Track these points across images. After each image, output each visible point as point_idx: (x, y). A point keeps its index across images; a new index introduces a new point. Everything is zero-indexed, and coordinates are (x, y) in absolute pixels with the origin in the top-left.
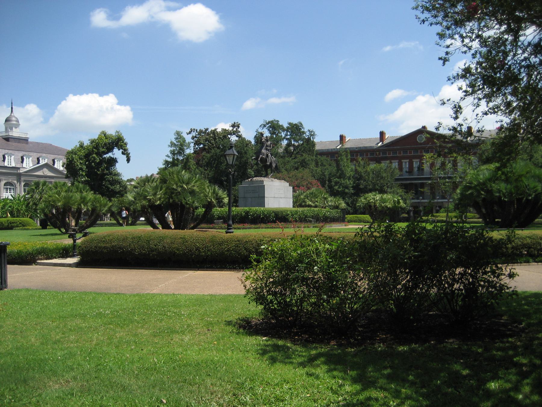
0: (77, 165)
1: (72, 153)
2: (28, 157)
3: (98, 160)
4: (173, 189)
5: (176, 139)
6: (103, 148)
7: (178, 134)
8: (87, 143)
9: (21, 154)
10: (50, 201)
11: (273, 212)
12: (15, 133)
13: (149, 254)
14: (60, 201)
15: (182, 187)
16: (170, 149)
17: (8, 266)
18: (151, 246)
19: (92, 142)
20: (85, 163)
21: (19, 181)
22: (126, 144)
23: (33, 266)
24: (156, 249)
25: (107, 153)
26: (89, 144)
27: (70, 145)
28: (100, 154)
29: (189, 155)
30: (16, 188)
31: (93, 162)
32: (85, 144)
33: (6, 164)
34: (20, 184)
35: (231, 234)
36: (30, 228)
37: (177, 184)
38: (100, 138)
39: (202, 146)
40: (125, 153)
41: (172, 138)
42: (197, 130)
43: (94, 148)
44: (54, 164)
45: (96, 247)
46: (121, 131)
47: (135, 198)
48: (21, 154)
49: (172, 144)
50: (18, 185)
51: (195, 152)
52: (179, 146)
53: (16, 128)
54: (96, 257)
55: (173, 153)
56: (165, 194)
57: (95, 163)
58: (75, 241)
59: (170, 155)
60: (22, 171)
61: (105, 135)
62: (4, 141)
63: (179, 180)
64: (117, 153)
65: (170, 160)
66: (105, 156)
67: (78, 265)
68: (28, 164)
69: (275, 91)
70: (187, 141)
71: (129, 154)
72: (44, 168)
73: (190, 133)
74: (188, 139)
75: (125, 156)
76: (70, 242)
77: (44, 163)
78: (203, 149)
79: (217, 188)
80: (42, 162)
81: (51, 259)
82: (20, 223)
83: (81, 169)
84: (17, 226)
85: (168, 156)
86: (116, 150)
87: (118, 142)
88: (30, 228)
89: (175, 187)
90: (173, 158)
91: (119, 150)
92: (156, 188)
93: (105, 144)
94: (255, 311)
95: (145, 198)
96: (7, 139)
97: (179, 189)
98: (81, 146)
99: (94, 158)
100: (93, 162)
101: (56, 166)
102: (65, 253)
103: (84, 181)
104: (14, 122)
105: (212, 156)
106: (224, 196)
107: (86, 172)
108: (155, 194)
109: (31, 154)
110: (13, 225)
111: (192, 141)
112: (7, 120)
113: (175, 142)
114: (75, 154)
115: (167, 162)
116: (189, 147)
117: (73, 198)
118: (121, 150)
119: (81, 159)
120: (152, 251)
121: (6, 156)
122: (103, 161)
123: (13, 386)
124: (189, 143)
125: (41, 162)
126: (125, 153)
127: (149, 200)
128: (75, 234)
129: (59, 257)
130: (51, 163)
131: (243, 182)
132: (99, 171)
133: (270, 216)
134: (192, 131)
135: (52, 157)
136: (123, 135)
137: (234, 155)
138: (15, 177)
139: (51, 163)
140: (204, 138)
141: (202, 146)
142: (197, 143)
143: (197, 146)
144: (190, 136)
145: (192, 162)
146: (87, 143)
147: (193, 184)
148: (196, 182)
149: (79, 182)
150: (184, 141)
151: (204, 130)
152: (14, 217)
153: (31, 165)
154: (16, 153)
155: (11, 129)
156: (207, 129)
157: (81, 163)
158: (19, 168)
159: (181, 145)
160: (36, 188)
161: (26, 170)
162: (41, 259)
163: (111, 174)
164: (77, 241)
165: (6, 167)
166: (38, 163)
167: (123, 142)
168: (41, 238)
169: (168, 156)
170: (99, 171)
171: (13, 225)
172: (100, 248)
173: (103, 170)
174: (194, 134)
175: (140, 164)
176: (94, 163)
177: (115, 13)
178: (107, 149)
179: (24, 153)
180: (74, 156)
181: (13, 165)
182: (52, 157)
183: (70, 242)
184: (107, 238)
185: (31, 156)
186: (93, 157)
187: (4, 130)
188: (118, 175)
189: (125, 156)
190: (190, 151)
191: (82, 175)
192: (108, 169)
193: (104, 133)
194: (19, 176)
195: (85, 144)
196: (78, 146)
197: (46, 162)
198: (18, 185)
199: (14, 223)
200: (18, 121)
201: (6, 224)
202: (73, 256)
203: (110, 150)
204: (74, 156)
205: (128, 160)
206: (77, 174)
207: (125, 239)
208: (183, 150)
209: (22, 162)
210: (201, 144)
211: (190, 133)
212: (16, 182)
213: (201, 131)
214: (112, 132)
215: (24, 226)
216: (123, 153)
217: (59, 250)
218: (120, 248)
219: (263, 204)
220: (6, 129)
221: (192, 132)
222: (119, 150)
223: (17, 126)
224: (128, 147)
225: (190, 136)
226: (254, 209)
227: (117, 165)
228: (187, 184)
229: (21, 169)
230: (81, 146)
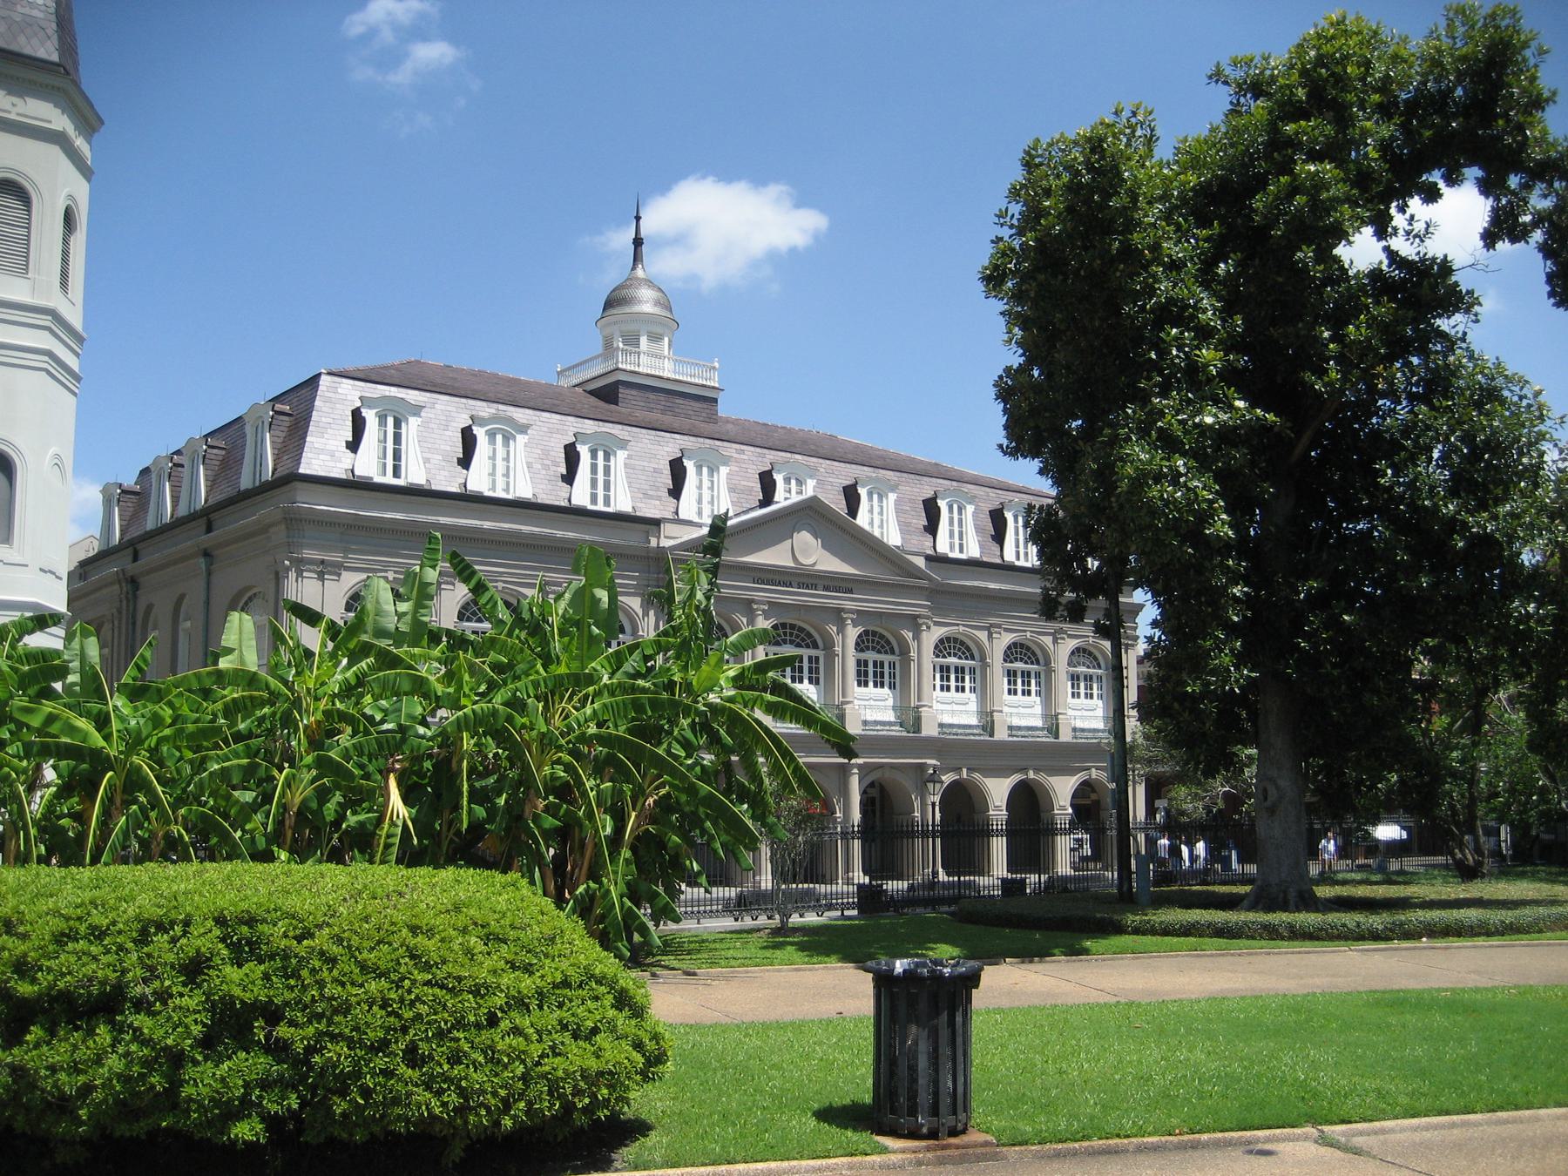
20: (1209, 264)
33: (580, 495)
36: (1438, 1020)
44: (853, 510)
48: (670, 446)
60: (671, 537)
62: (593, 400)
69: (246, 1130)
72: (796, 528)
77: (795, 498)
80: (785, 497)
101: (862, 520)
103: (1224, 436)
109: (730, 449)
125: (780, 495)
136: (1525, 24)
149: (1169, 444)
154: (644, 440)
155: (632, 340)
158: (656, 523)
166: (767, 500)
168: (676, 425)
181: (622, 502)
182: (845, 474)
185: (726, 461)
191: (1193, 370)
220: (608, 345)
229: (667, 529)
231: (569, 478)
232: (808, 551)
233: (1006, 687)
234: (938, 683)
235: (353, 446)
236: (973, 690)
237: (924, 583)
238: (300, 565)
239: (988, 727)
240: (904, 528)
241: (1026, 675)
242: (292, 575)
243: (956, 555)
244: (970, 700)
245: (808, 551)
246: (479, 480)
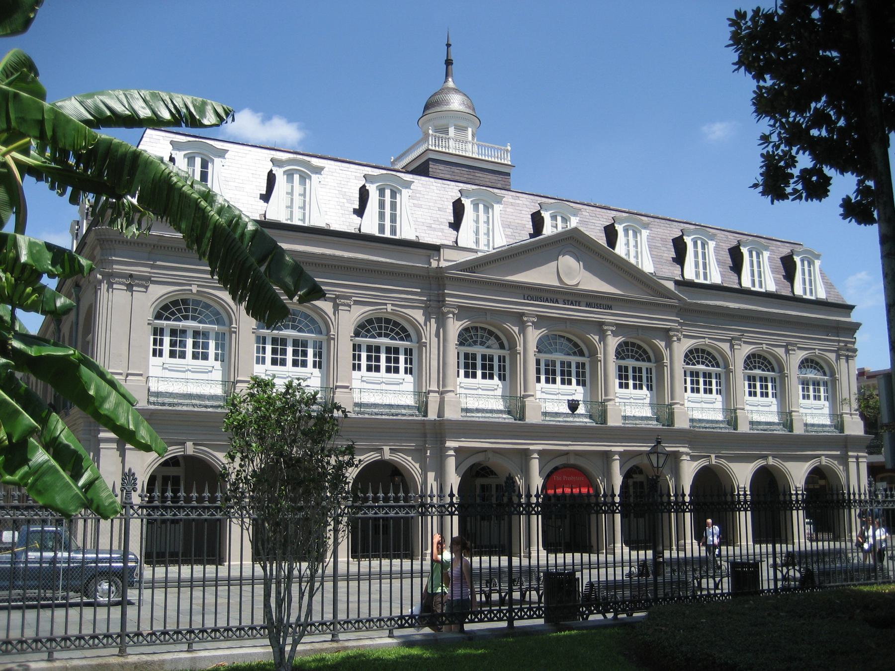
21: (436, 309)
34: (442, 323)
60: (448, 259)
138: (414, 293)
158: (436, 249)
161: (471, 256)
193: (740, 63)
212: (418, 315)
229: (446, 254)
233: (801, 393)
234: (689, 386)
236: (719, 392)
237: (674, 302)
238: (110, 277)
239: (733, 422)
241: (764, 379)
242: (104, 286)
244: (772, 403)
245: (571, 272)
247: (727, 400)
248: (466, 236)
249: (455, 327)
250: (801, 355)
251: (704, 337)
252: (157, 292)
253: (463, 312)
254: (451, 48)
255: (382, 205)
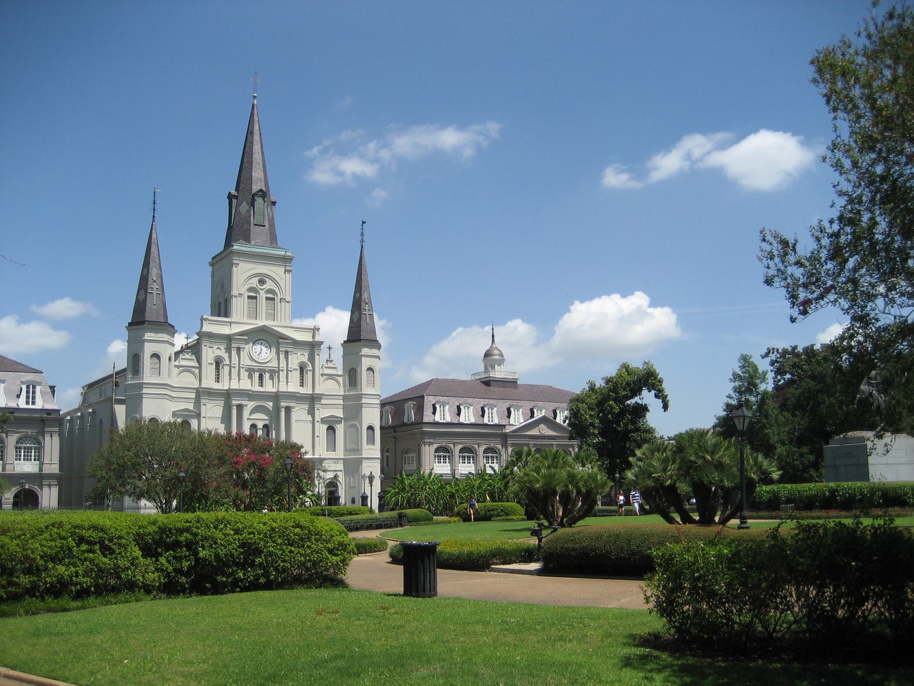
0: (586, 419)
1: (577, 400)
2: (517, 408)
3: (617, 410)
4: (691, 461)
5: (742, 367)
6: (625, 389)
7: (745, 361)
8: (599, 383)
9: (506, 404)
10: (525, 482)
11: (879, 489)
12: (499, 373)
13: (630, 558)
14: (538, 481)
15: (704, 458)
16: (733, 384)
17: (439, 571)
18: (632, 547)
19: (608, 381)
21: (505, 445)
22: (660, 381)
23: (487, 573)
24: (638, 552)
25: (632, 397)
26: (603, 385)
27: (578, 387)
28: (620, 400)
29: (765, 393)
30: (500, 455)
31: (609, 413)
32: (598, 386)
33: (486, 421)
34: (506, 449)
35: (745, 530)
36: (515, 518)
37: (696, 454)
38: (619, 376)
39: (788, 376)
40: (660, 395)
41: (736, 367)
42: (778, 350)
43: (611, 390)
44: (555, 417)
45: (561, 548)
46: (652, 362)
47: (636, 476)
48: (506, 404)
49: (736, 377)
50: (503, 451)
51: (777, 388)
52: (748, 379)
53: (499, 365)
54: (561, 563)
55: (738, 390)
56: (680, 468)
57: (613, 414)
58: (540, 541)
59: (733, 395)
60: (508, 430)
61: (627, 370)
63: (700, 447)
64: (647, 397)
65: (734, 402)
66: (629, 402)
67: (539, 573)
68: (518, 419)
70: (760, 371)
71: (666, 397)
73: (767, 355)
74: (764, 366)
75: (660, 401)
76: (534, 541)
77: (540, 416)
78: (791, 382)
79: (760, 458)
80: (538, 415)
81: (510, 563)
82: (502, 511)
83: (592, 425)
84: (498, 515)
85: (729, 397)
86: (645, 392)
87: (648, 379)
88: (515, 518)
89: (693, 458)
90: (739, 401)
91: (650, 391)
92: (665, 461)
93: (628, 384)
94: (658, 624)
95: (650, 476)
96: (487, 383)
97: (700, 462)
98: (592, 388)
99: (611, 406)
100: (609, 413)
102: (527, 555)
104: (497, 357)
105: (803, 393)
106: (772, 469)
107: (599, 429)
108: (664, 470)
110: (492, 513)
111: (772, 368)
112: (487, 355)
113: (740, 373)
114: (583, 402)
115: (729, 407)
116: (764, 378)
117: (557, 477)
118: (653, 392)
119: (590, 409)
120: (634, 554)
121: (486, 409)
122: (625, 410)
123: (392, 668)
124: (765, 373)
126: (660, 395)
127: (657, 480)
128: (540, 531)
129: (520, 562)
130: (551, 416)
131: (831, 441)
132: (620, 426)
133: (872, 495)
134: (769, 352)
135: (553, 406)
137: (744, 417)
138: (499, 440)
139: (551, 416)
140: (791, 363)
141: (788, 376)
142: (779, 372)
143: (779, 377)
144: (768, 360)
145: (771, 404)
146: (599, 383)
147: (721, 453)
148: (725, 450)
149: (589, 445)
150: (756, 369)
151: (790, 349)
152: (495, 501)
153: (522, 420)
155: (493, 368)
156: (795, 348)
157: (591, 415)
158: (504, 426)
159: (751, 377)
160: (517, 459)
161: (514, 428)
162: (497, 564)
163: (637, 430)
164: (543, 540)
165: (486, 425)
166: (532, 416)
167: (655, 378)
169: (729, 397)
170: (620, 426)
171: (492, 513)
172: (567, 549)
173: (626, 425)
174: (773, 357)
175: (687, 410)
176: (612, 414)
177: (639, 169)
178: (630, 391)
179: (511, 402)
180: (580, 405)
182: (553, 406)
183: (534, 541)
184: (576, 536)
185: (521, 407)
186: (609, 405)
187: (482, 368)
188: (650, 431)
189: (660, 401)
190: (767, 386)
192: (634, 422)
193: (626, 367)
194: (504, 438)
195: (598, 386)
196: (587, 389)
197: (543, 414)
198: (503, 451)
199: (492, 510)
200: (502, 355)
201: (483, 512)
202: (535, 561)
203: (636, 391)
204: (580, 405)
205: (665, 407)
206: (587, 433)
207: (599, 537)
208: (756, 386)
209: (509, 416)
210: (786, 373)
211: (767, 355)
212: (500, 447)
213: (785, 352)
214: (637, 364)
215: (507, 514)
216: (656, 396)
217: (520, 552)
218: (592, 550)
219: (865, 476)
220: (486, 368)
221: (771, 354)
222: (650, 391)
223: (501, 362)
224: (664, 385)
225: (768, 360)
226: (845, 484)
227: (648, 415)
228: (712, 453)
229: (507, 427)
230: (592, 388)
231: (483, 416)
232: (545, 430)
235: (434, 413)
239: (453, 474)
240: (500, 418)
241: (469, 457)
243: (442, 421)
245: (545, 430)
246: (462, 419)
247: (452, 466)
248: (512, 421)
249: (510, 449)
250: (484, 447)
251: (468, 442)
252: (435, 446)
253: (513, 445)
254: (367, 358)
255: (28, 392)
